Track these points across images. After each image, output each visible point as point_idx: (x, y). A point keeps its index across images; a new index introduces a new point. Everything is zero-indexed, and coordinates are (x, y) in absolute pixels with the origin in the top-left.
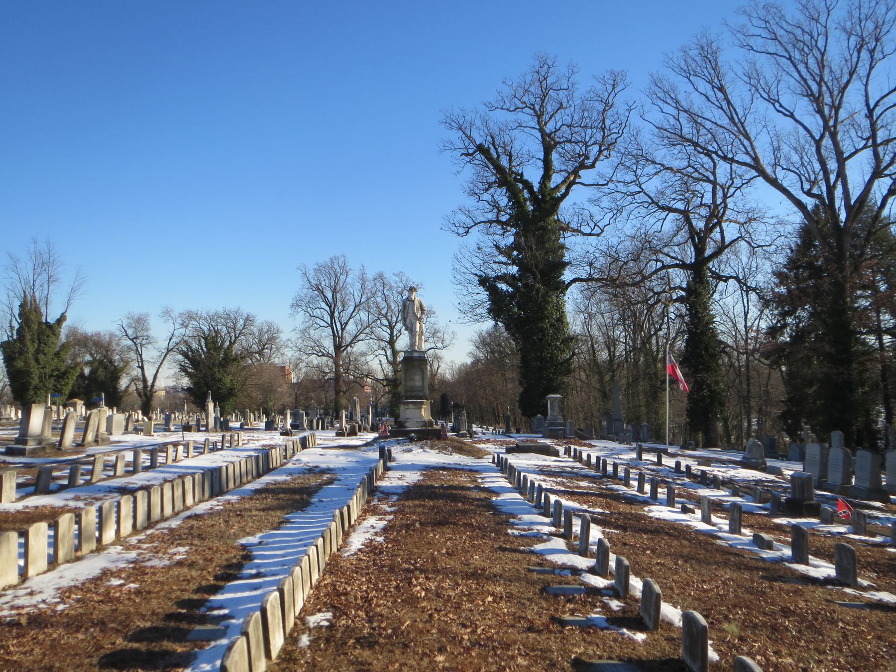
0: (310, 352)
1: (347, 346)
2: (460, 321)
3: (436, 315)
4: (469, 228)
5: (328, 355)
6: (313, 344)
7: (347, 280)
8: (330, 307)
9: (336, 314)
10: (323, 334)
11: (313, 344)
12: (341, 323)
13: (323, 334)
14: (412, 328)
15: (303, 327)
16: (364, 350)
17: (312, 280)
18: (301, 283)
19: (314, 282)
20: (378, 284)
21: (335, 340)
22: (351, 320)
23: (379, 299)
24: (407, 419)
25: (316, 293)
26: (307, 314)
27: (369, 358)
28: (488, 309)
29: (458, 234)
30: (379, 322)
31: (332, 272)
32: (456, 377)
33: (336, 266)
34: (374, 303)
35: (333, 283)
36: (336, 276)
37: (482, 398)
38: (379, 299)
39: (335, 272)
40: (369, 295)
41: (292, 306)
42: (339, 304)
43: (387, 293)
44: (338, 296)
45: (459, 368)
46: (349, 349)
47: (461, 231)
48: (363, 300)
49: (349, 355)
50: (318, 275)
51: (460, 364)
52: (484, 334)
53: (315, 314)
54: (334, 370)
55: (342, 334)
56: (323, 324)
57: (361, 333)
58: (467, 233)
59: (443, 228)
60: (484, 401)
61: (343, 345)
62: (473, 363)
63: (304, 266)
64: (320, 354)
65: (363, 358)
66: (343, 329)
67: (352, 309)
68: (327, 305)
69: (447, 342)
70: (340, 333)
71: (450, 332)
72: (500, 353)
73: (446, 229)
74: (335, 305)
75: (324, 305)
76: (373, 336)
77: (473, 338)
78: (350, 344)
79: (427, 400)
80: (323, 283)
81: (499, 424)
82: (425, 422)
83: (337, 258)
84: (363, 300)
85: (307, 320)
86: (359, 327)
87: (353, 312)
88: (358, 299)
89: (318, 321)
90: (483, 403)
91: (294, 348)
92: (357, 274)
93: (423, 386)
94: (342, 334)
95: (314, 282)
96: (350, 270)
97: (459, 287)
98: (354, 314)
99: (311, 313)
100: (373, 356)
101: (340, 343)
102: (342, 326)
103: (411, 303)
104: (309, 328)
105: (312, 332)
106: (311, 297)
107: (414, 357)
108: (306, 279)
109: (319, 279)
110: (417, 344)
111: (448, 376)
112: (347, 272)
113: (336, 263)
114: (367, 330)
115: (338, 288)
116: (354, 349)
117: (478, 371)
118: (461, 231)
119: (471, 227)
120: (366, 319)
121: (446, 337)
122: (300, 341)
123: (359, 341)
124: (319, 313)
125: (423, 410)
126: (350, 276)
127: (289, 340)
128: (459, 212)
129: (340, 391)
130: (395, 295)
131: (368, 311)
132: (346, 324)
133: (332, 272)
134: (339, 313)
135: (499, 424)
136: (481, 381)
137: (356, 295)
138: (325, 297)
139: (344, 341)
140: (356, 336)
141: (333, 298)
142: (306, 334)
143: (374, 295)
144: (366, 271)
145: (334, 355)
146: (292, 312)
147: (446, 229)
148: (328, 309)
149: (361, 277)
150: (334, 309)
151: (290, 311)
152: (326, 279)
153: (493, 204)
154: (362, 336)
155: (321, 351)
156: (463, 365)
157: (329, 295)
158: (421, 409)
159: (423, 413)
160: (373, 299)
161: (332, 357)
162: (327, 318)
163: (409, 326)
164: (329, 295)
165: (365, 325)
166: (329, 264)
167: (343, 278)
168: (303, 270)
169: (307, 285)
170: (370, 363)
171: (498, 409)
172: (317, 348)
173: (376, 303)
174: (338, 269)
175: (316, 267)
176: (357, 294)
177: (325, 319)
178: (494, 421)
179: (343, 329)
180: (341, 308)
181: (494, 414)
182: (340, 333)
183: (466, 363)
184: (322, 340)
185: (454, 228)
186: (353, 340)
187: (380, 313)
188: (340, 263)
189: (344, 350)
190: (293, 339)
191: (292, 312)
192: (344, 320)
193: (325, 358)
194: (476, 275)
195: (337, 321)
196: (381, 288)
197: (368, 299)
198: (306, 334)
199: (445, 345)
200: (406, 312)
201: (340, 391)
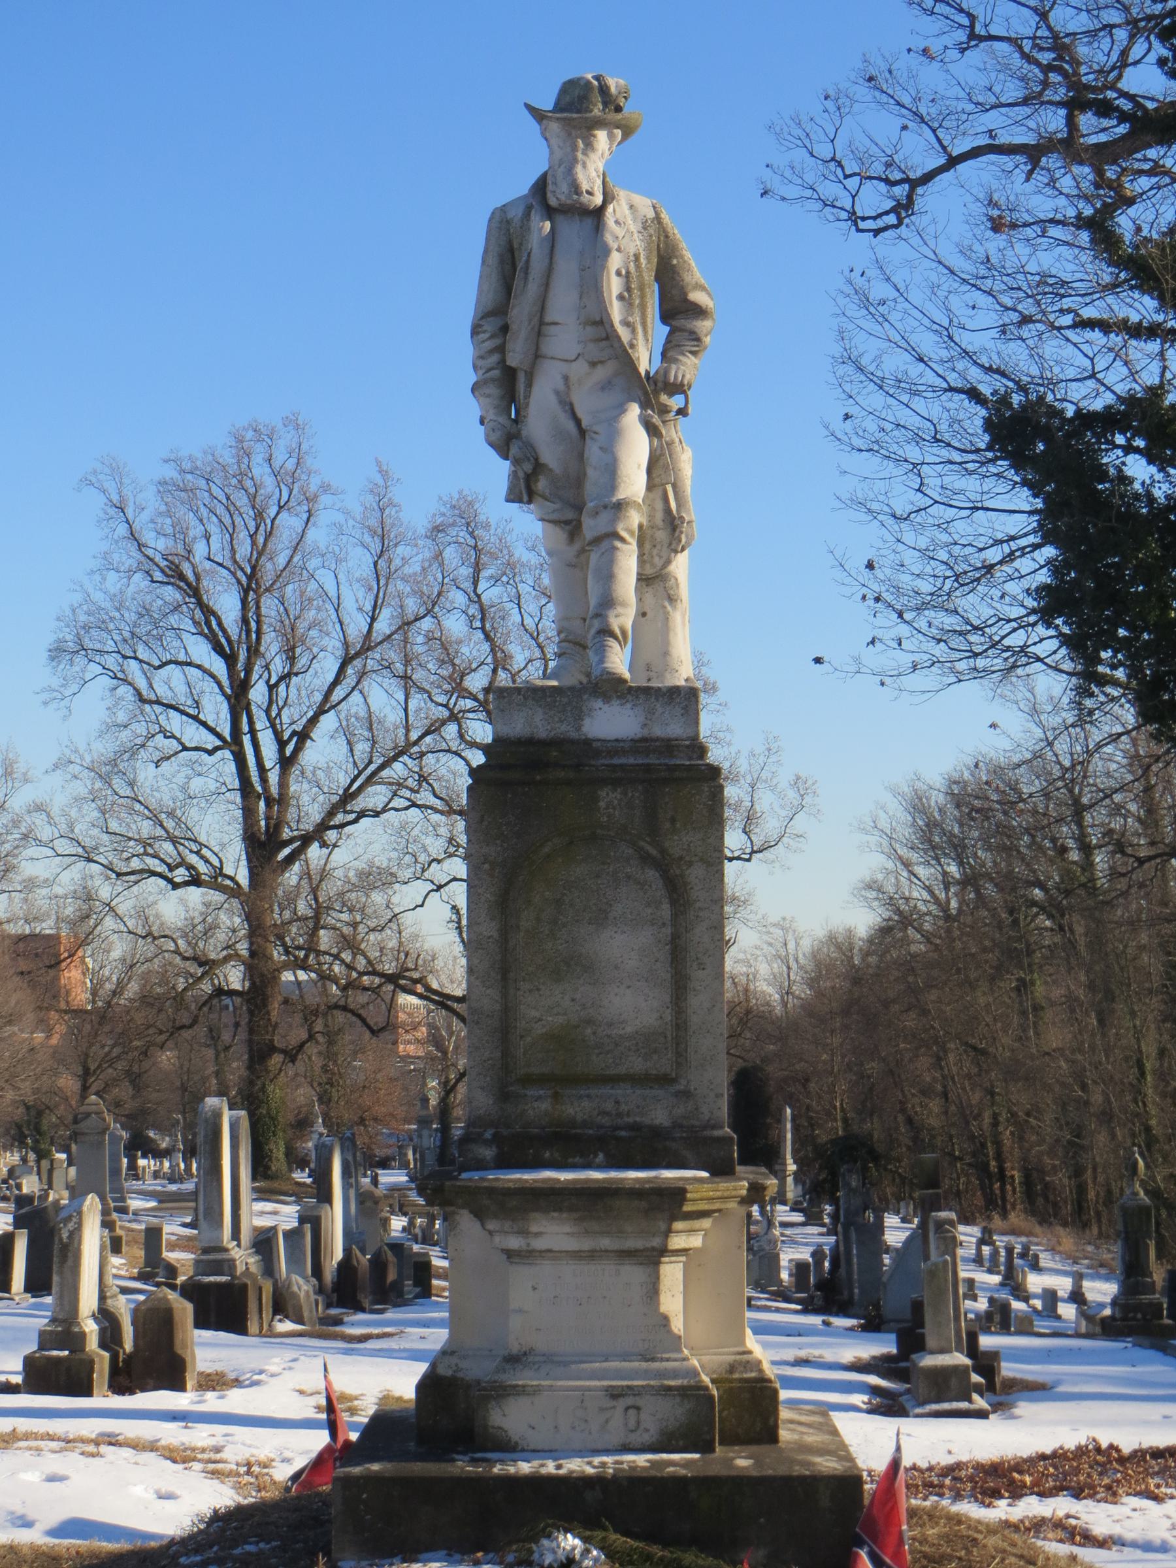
0: (135, 864)
1: (306, 840)
2: (875, 658)
3: (721, 696)
4: (914, 184)
5: (217, 880)
6: (146, 828)
7: (312, 534)
8: (230, 659)
9: (258, 694)
10: (196, 785)
11: (146, 828)
12: (278, 735)
13: (196, 785)
14: (579, 481)
15: (104, 748)
16: (382, 861)
17: (149, 537)
18: (104, 546)
19: (162, 544)
20: (450, 554)
21: (248, 813)
22: (328, 722)
23: (455, 625)
24: (514, 1360)
25: (171, 594)
26: (124, 690)
27: (406, 895)
28: (1043, 589)
29: (854, 218)
30: (451, 730)
31: (241, 500)
32: (802, 991)
33: (260, 471)
34: (429, 638)
35: (244, 549)
36: (259, 516)
37: (926, 1092)
38: (455, 625)
39: (252, 498)
40: (412, 606)
41: (57, 652)
42: (271, 645)
43: (490, 593)
44: (269, 606)
45: (814, 955)
46: (314, 852)
47: (874, 199)
48: (383, 626)
49: (315, 881)
50: (181, 511)
51: (821, 933)
52: (938, 798)
53: (162, 691)
54: (243, 948)
55: (283, 784)
56: (194, 735)
57: (369, 781)
58: (903, 209)
59: (775, 183)
60: (935, 1105)
61: (286, 833)
62: (885, 931)
63: (116, 472)
64: (180, 874)
65: (377, 897)
66: (286, 763)
67: (328, 667)
68: (218, 648)
69: (768, 828)
70: (273, 777)
71: (784, 778)
72: (1008, 883)
73: (792, 192)
74: (254, 651)
75: (201, 651)
76: (425, 797)
77: (884, 823)
78: (317, 834)
79: (721, 1170)
80: (200, 550)
81: (1004, 1215)
82: (693, 1393)
83: (264, 435)
84: (383, 626)
85: (122, 717)
86: (362, 748)
87: (336, 682)
88: (357, 626)
89: (175, 722)
90: (932, 1113)
91: (63, 846)
92: (357, 511)
93: (680, 1025)
94: (283, 784)
95: (159, 545)
96: (326, 488)
97: (870, 465)
98: (338, 693)
99: (142, 684)
100: (423, 887)
101: (275, 828)
102: (282, 744)
103: (572, 232)
104: (133, 751)
105: (146, 774)
106: (145, 612)
107: (588, 746)
108: (122, 530)
109: (180, 532)
110: (624, 618)
111: (767, 989)
112: (311, 500)
113: (258, 459)
114: (398, 769)
115: (268, 571)
116: (340, 857)
117: (909, 965)
118: (874, 199)
119: (927, 178)
120: (394, 716)
121: (765, 801)
122: (91, 813)
123: (361, 815)
124: (181, 689)
125: (672, 1273)
126: (324, 518)
127: (39, 808)
128: (862, 91)
129: (272, 1049)
130: (530, 606)
131: (406, 677)
132: (303, 736)
133: (241, 500)
134: (271, 688)
135: (1004, 1215)
136: (925, 1012)
137: (348, 604)
138: (208, 611)
139: (291, 814)
140: (348, 796)
141: (245, 621)
142: (117, 782)
143: (431, 607)
144: (396, 493)
145: (243, 878)
146: (55, 682)
147: (792, 192)
148: (219, 667)
149: (374, 522)
150: (248, 670)
151: (43, 675)
152: (214, 529)
153: (1046, 57)
154: (375, 796)
155: (183, 863)
156: (832, 938)
157: (228, 605)
158: (654, 1257)
159: (672, 1302)
160: (427, 624)
161: (234, 891)
162: (217, 710)
163: (550, 456)
164: (228, 605)
165: (386, 744)
166: (228, 457)
167: (289, 524)
168: (111, 486)
169: (128, 557)
170: (408, 919)
171: (998, 1144)
172: (168, 847)
173: (446, 649)
174: (269, 482)
175: (170, 473)
176: (355, 603)
177: (208, 716)
178: (979, 1200)
179: (286, 763)
180: (278, 666)
181: (983, 1168)
182: (273, 777)
183: (850, 932)
184: (192, 814)
185: (830, 190)
186: (331, 814)
187: (459, 689)
188: (279, 458)
189: (290, 860)
190: (58, 803)
191: (55, 682)
192: (292, 717)
193: (195, 895)
194: (974, 394)
195: (261, 723)
196: (465, 572)
197: (406, 625)
198: (117, 782)
199: (758, 841)
200: (521, 313)
201: (272, 1049)
